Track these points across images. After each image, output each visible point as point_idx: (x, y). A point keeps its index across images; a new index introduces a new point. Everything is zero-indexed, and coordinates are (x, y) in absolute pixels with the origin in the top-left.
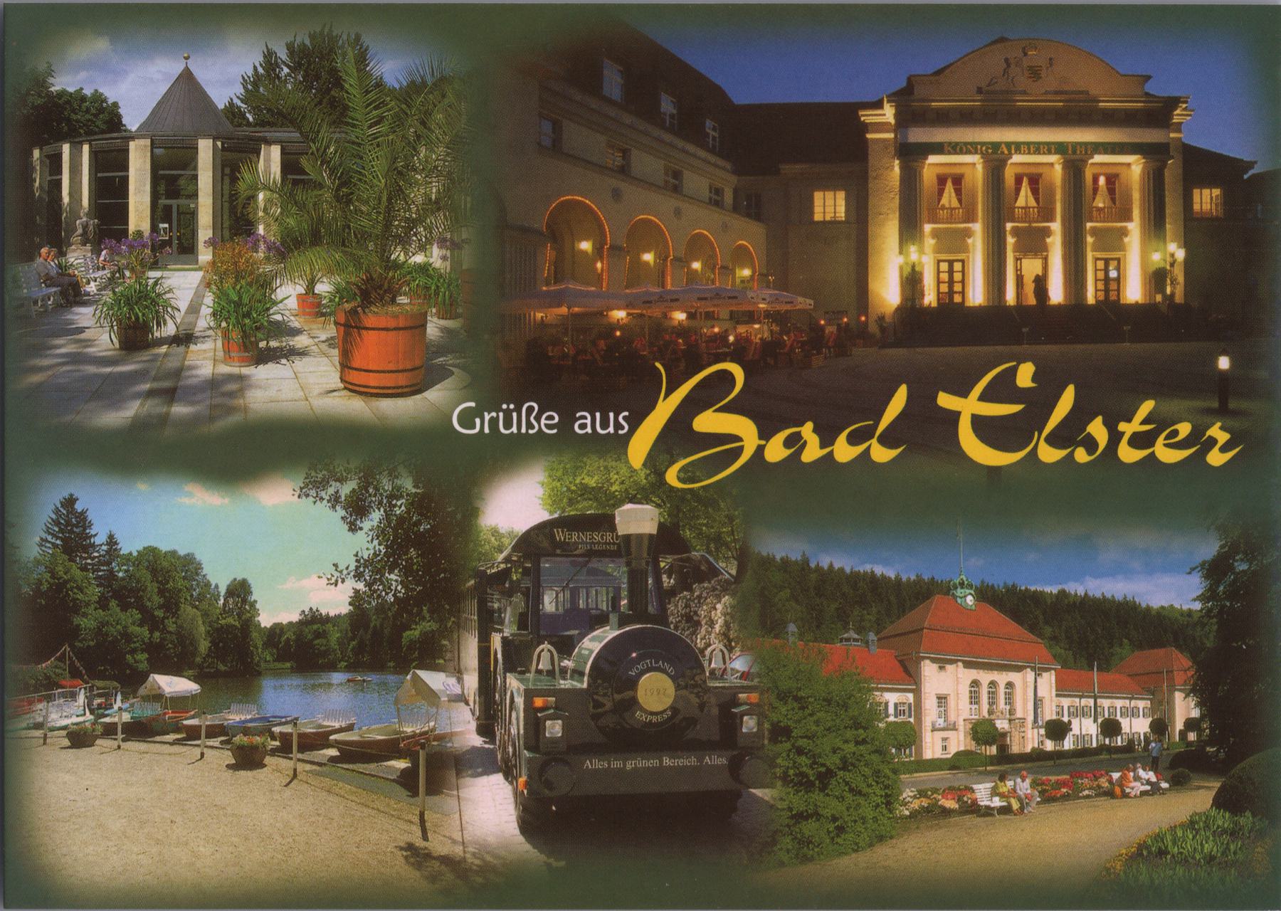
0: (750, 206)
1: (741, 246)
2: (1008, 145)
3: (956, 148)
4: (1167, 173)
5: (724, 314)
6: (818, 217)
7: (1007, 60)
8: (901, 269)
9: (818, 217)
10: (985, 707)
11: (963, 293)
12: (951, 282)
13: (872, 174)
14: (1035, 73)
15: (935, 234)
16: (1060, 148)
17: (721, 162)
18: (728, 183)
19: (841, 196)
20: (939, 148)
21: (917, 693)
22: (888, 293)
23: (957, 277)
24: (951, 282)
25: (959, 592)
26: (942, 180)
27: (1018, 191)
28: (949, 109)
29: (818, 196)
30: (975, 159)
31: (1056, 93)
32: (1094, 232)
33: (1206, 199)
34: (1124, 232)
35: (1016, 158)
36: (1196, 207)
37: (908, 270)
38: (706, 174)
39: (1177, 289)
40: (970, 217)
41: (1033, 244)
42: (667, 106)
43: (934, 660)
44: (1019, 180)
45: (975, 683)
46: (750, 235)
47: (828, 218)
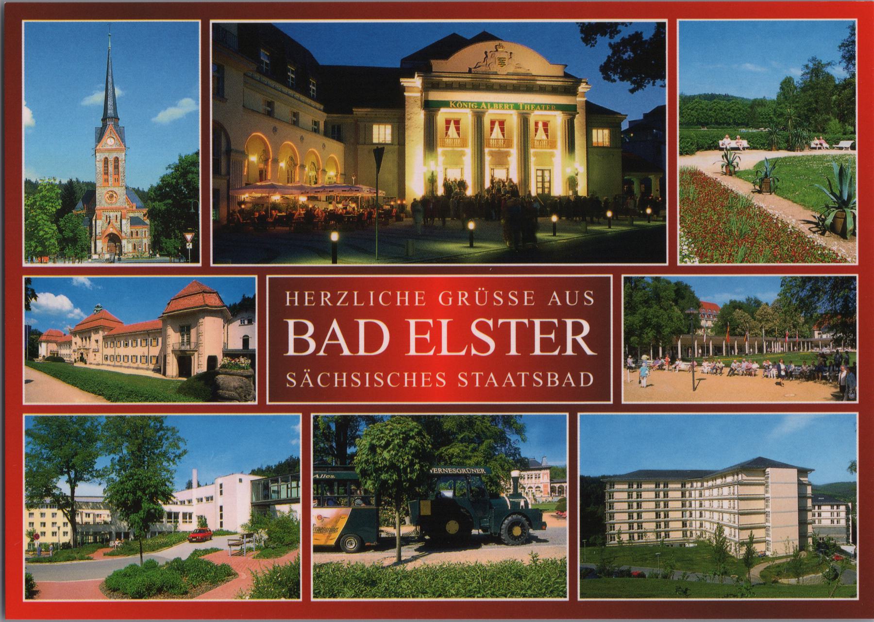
0: (334, 132)
1: (332, 158)
2: (486, 103)
3: (457, 105)
4: (576, 121)
5: (323, 198)
6: (375, 141)
7: (486, 53)
8: (425, 174)
9: (375, 141)
11: (550, 188)
12: (543, 182)
13: (407, 116)
14: (502, 62)
15: (445, 154)
16: (516, 106)
17: (318, 105)
18: (321, 117)
20: (446, 104)
22: (416, 189)
23: (547, 179)
24: (543, 182)
26: (448, 122)
27: (492, 129)
28: (452, 82)
29: (375, 128)
31: (513, 74)
33: (601, 136)
34: (552, 155)
35: (490, 111)
36: (594, 140)
38: (313, 113)
39: (582, 190)
40: (464, 145)
41: (501, 159)
42: (264, 56)
44: (493, 123)
46: (335, 150)
47: (381, 141)
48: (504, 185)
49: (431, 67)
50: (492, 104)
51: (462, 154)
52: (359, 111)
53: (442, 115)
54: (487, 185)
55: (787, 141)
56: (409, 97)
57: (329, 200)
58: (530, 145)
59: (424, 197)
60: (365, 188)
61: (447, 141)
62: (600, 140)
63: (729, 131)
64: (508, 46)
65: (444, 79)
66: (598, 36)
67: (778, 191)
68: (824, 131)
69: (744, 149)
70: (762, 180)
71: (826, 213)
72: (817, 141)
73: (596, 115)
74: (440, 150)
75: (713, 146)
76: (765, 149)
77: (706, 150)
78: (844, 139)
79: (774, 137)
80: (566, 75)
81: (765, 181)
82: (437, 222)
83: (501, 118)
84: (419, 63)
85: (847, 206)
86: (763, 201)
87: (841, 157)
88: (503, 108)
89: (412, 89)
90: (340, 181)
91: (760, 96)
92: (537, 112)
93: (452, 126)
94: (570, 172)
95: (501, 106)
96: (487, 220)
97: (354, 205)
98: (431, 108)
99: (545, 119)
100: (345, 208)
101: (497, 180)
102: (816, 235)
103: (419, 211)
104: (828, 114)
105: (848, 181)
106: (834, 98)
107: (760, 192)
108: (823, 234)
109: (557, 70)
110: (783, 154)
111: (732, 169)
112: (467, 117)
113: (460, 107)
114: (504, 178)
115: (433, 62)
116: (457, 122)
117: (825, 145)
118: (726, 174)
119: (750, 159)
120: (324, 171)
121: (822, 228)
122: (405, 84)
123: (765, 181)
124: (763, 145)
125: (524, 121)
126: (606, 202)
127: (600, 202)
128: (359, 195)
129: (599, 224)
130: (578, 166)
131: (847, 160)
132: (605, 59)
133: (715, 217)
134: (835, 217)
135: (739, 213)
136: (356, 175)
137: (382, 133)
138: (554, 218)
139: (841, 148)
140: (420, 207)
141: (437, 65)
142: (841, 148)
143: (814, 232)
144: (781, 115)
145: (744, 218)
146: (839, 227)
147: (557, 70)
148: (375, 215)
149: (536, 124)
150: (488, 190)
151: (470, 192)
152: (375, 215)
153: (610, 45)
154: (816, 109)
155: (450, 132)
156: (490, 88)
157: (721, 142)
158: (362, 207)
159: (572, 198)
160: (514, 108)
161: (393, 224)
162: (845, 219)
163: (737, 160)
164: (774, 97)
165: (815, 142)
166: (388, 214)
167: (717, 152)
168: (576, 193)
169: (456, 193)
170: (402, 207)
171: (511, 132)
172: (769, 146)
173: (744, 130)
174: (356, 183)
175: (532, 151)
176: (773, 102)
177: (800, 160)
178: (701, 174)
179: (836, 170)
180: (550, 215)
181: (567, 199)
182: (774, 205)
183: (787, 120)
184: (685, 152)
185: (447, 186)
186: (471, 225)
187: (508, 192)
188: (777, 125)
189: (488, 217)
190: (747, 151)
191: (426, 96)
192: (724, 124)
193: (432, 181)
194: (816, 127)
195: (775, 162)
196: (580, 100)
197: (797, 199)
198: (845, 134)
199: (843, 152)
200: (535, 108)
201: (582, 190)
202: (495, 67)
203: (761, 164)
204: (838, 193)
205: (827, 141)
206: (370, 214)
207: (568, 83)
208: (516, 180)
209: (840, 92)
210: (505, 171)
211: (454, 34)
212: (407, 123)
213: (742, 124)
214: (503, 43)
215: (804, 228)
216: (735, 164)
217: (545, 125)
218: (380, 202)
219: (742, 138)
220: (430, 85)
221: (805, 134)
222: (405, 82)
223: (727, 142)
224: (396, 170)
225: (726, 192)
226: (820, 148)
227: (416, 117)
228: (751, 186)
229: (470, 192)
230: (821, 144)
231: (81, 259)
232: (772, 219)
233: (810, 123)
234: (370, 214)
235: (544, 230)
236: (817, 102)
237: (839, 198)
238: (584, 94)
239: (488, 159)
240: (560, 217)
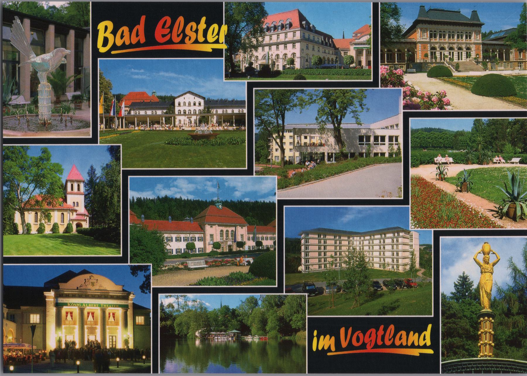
0: (12, 318)
2: (85, 304)
3: (71, 305)
6: (31, 322)
8: (56, 338)
9: (31, 322)
10: (225, 237)
11: (116, 345)
12: (112, 342)
14: (93, 284)
15: (66, 328)
16: (100, 305)
19: (38, 316)
20: (66, 304)
21: (204, 234)
22: (51, 345)
23: (114, 340)
24: (112, 342)
25: (217, 204)
26: (67, 313)
27: (88, 316)
28: (69, 294)
29: (32, 316)
30: (77, 307)
33: (140, 320)
34: (117, 329)
35: (88, 308)
36: (137, 321)
37: (58, 338)
39: (131, 346)
40: (75, 324)
41: (92, 331)
43: (209, 225)
44: (88, 313)
45: (222, 231)
48: (94, 343)
49: (59, 286)
50: (88, 304)
51: (74, 328)
52: (23, 308)
53: (64, 309)
54: (86, 343)
55: (478, 158)
56: (48, 301)
57: (9, 350)
58: (106, 323)
59: (55, 349)
60: (27, 345)
61: (67, 322)
62: (140, 321)
63: (441, 151)
64: (96, 276)
65: (65, 292)
66: (139, 272)
67: (473, 191)
68: (502, 152)
69: (450, 163)
70: (462, 183)
71: (504, 205)
72: (497, 158)
73: (138, 310)
74: (63, 326)
75: (431, 162)
76: (464, 164)
77: (426, 164)
78: (515, 157)
79: (469, 156)
80: (124, 290)
81: (464, 184)
82: (62, 361)
83: (93, 311)
84: (53, 284)
85: (517, 200)
86: (463, 197)
87: (513, 168)
88: (93, 306)
89: (49, 297)
90: (14, 342)
91: (460, 129)
92: (109, 308)
93: (69, 315)
94: (125, 337)
95: (93, 305)
96: (85, 360)
97: (21, 353)
98: (58, 306)
99: (114, 311)
100: (17, 355)
101: (90, 341)
102: (497, 219)
103: (53, 356)
104: (504, 140)
105: (518, 184)
106: (508, 130)
107: (460, 191)
108: (501, 218)
109: (119, 288)
110: (476, 166)
111: (442, 176)
112: (76, 311)
113: (73, 306)
114: (94, 340)
115: (60, 284)
116: (71, 313)
117: (503, 161)
118: (439, 180)
119: (454, 170)
120: (7, 337)
121: (501, 215)
122: (46, 295)
123: (464, 184)
124: (463, 160)
125: (104, 312)
126: (143, 352)
127: (139, 352)
128: (24, 348)
129: (139, 362)
130: (129, 334)
131: (517, 170)
132: (142, 283)
133: (432, 208)
134: (509, 207)
135: (448, 204)
136: (22, 338)
137: (35, 318)
138: (118, 359)
139: (513, 163)
140: (53, 354)
141: (62, 286)
142: (513, 163)
143: (496, 217)
144: (474, 141)
145: (451, 208)
146: (512, 213)
147: (119, 288)
148: (31, 358)
149: (109, 314)
150: (86, 346)
151: (77, 347)
152: (31, 358)
153: (144, 276)
154: (497, 138)
155: (68, 318)
156: (87, 296)
157: (435, 159)
158: (25, 354)
159: (126, 350)
160: (99, 306)
161: (40, 362)
162: (516, 208)
163: (446, 170)
164: (470, 130)
165: (496, 159)
166: (38, 357)
167: (433, 165)
168: (128, 347)
169: (71, 348)
170: (45, 354)
171: (97, 318)
172: (467, 162)
173: (450, 151)
174: (22, 342)
175: (107, 327)
176: (468, 133)
177: (486, 171)
178: (423, 179)
179: (510, 177)
180: (116, 358)
181: (123, 350)
182: (469, 199)
183: (478, 145)
184: (414, 166)
185: (67, 344)
186: (78, 363)
187: (96, 347)
188: (472, 148)
189: (86, 359)
190: (452, 165)
191: (57, 300)
192: (437, 147)
193: (60, 341)
194: (497, 149)
195: (470, 172)
196: (130, 302)
197: (484, 196)
198: (515, 154)
199: (514, 165)
200: (109, 306)
201: (131, 346)
202: (90, 287)
203: (461, 173)
204: (511, 192)
205: (504, 158)
206: (29, 357)
207: (125, 294)
208: (99, 341)
209: (512, 127)
210: (94, 337)
211: (70, 271)
212: (47, 313)
213: (449, 147)
214: (94, 275)
215: (489, 214)
216: (444, 173)
217: (114, 314)
218: (34, 351)
219: (449, 156)
220: (58, 295)
221: (490, 153)
222: (46, 294)
223: (439, 159)
224: (41, 336)
225: (439, 191)
226: (499, 163)
227: (52, 311)
228: (454, 187)
229: (77, 347)
230: (500, 160)
231: (112, 146)
232: (468, 208)
233: (493, 147)
234: (29, 357)
235: (113, 365)
236: (497, 133)
237: (512, 195)
238: (132, 300)
239: (86, 331)
240: (120, 359)
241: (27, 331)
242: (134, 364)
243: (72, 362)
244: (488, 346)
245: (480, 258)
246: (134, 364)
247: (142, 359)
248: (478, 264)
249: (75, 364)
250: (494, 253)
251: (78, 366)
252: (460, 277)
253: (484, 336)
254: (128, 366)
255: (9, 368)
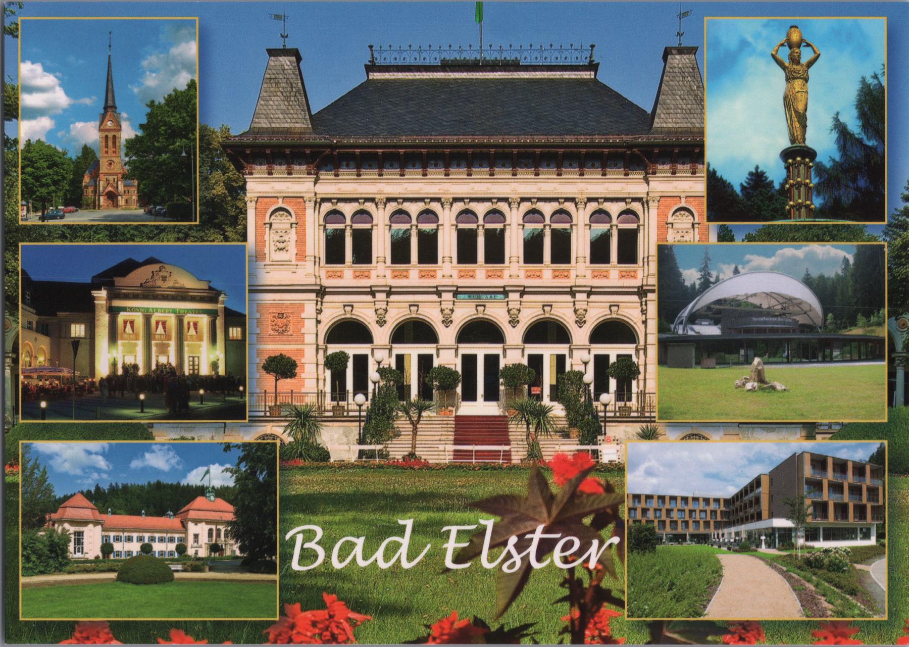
0: (43, 329)
3: (132, 309)
6: (73, 335)
9: (73, 335)
11: (198, 369)
12: (193, 365)
14: (164, 279)
15: (123, 345)
16: (174, 311)
17: (31, 310)
18: (34, 319)
19: (83, 327)
20: (124, 309)
22: (102, 370)
23: (196, 363)
24: (193, 365)
26: (125, 322)
27: (157, 328)
29: (73, 326)
30: (140, 314)
31: (173, 288)
32: (188, 345)
34: (200, 346)
36: (231, 335)
39: (222, 371)
40: (137, 339)
41: (163, 349)
44: (157, 323)
45: (210, 530)
46: (44, 343)
51: (135, 345)
53: (122, 317)
54: (154, 367)
57: (40, 378)
58: (185, 338)
59: (108, 376)
60: (65, 370)
62: (235, 335)
64: (169, 268)
74: (120, 342)
80: (210, 288)
84: (106, 279)
89: (100, 298)
90: (47, 364)
92: (189, 315)
93: (128, 325)
94: (213, 358)
95: (164, 311)
98: (113, 312)
99: (195, 320)
109: (203, 285)
112: (139, 319)
113: (134, 312)
116: (132, 323)
128: (61, 374)
129: (234, 396)
130: (219, 353)
136: (59, 360)
138: (202, 392)
140: (105, 383)
141: (119, 281)
149: (189, 323)
150: (154, 371)
151: (141, 373)
166: (82, 388)
168: (217, 373)
170: (93, 383)
175: (186, 343)
185: (125, 368)
191: (110, 303)
193: (114, 365)
196: (220, 306)
202: (159, 283)
206: (69, 388)
212: (97, 323)
220: (111, 297)
222: (95, 293)
227: (103, 319)
229: (141, 373)
234: (69, 388)
235: (194, 400)
238: (223, 302)
239: (154, 349)
240: (205, 391)
241: (67, 349)
242: (227, 398)
243: (134, 395)
244: (802, 189)
245: (784, 54)
246: (227, 398)
247: (238, 390)
248: (780, 64)
249: (137, 398)
250: (808, 45)
251: (142, 401)
252: (751, 174)
253: (796, 192)
254: (217, 401)
255: (39, 404)
